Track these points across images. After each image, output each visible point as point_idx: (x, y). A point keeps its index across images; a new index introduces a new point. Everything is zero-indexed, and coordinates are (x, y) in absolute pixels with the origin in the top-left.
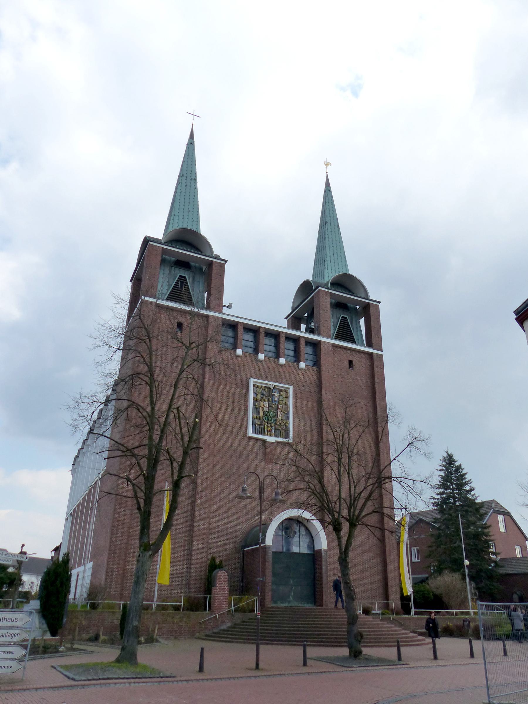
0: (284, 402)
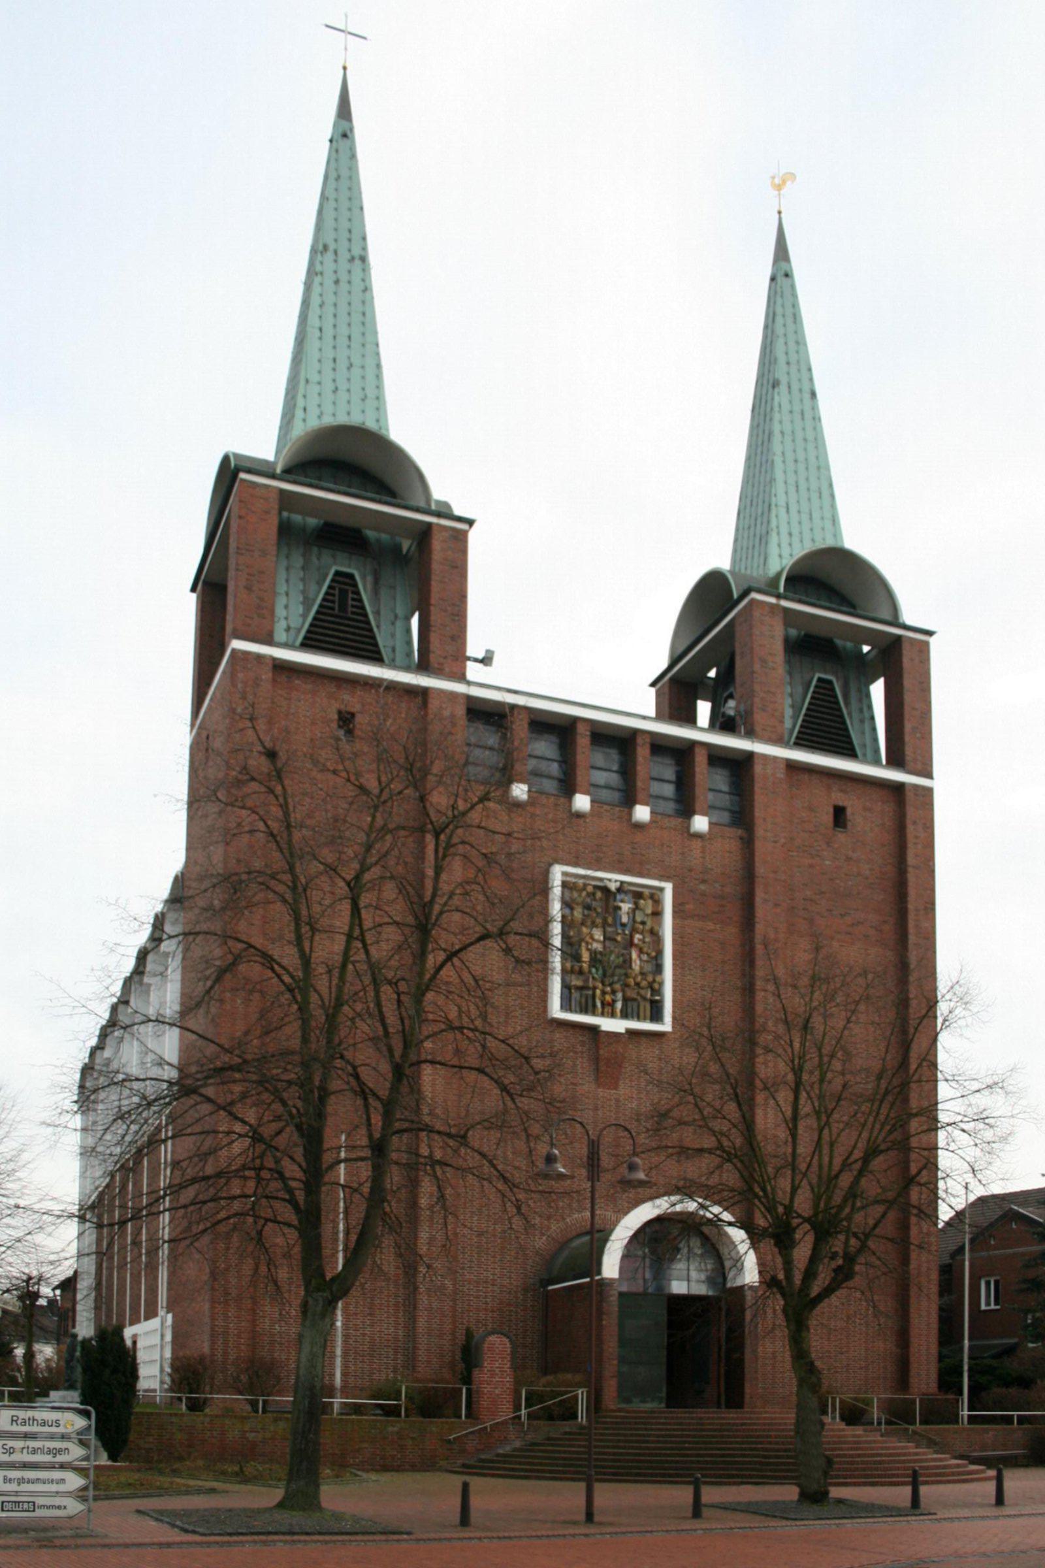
0: (648, 927)
